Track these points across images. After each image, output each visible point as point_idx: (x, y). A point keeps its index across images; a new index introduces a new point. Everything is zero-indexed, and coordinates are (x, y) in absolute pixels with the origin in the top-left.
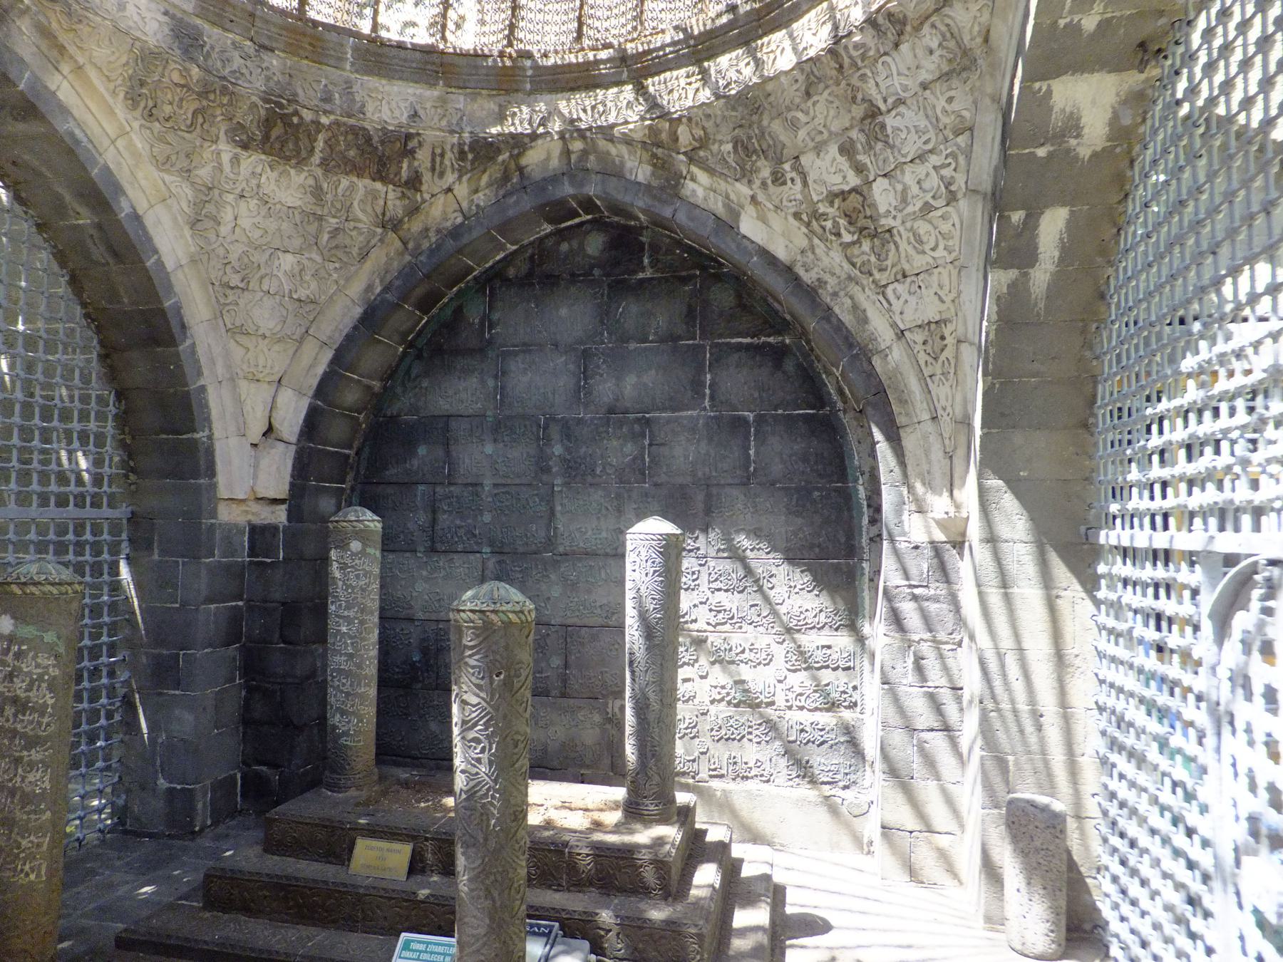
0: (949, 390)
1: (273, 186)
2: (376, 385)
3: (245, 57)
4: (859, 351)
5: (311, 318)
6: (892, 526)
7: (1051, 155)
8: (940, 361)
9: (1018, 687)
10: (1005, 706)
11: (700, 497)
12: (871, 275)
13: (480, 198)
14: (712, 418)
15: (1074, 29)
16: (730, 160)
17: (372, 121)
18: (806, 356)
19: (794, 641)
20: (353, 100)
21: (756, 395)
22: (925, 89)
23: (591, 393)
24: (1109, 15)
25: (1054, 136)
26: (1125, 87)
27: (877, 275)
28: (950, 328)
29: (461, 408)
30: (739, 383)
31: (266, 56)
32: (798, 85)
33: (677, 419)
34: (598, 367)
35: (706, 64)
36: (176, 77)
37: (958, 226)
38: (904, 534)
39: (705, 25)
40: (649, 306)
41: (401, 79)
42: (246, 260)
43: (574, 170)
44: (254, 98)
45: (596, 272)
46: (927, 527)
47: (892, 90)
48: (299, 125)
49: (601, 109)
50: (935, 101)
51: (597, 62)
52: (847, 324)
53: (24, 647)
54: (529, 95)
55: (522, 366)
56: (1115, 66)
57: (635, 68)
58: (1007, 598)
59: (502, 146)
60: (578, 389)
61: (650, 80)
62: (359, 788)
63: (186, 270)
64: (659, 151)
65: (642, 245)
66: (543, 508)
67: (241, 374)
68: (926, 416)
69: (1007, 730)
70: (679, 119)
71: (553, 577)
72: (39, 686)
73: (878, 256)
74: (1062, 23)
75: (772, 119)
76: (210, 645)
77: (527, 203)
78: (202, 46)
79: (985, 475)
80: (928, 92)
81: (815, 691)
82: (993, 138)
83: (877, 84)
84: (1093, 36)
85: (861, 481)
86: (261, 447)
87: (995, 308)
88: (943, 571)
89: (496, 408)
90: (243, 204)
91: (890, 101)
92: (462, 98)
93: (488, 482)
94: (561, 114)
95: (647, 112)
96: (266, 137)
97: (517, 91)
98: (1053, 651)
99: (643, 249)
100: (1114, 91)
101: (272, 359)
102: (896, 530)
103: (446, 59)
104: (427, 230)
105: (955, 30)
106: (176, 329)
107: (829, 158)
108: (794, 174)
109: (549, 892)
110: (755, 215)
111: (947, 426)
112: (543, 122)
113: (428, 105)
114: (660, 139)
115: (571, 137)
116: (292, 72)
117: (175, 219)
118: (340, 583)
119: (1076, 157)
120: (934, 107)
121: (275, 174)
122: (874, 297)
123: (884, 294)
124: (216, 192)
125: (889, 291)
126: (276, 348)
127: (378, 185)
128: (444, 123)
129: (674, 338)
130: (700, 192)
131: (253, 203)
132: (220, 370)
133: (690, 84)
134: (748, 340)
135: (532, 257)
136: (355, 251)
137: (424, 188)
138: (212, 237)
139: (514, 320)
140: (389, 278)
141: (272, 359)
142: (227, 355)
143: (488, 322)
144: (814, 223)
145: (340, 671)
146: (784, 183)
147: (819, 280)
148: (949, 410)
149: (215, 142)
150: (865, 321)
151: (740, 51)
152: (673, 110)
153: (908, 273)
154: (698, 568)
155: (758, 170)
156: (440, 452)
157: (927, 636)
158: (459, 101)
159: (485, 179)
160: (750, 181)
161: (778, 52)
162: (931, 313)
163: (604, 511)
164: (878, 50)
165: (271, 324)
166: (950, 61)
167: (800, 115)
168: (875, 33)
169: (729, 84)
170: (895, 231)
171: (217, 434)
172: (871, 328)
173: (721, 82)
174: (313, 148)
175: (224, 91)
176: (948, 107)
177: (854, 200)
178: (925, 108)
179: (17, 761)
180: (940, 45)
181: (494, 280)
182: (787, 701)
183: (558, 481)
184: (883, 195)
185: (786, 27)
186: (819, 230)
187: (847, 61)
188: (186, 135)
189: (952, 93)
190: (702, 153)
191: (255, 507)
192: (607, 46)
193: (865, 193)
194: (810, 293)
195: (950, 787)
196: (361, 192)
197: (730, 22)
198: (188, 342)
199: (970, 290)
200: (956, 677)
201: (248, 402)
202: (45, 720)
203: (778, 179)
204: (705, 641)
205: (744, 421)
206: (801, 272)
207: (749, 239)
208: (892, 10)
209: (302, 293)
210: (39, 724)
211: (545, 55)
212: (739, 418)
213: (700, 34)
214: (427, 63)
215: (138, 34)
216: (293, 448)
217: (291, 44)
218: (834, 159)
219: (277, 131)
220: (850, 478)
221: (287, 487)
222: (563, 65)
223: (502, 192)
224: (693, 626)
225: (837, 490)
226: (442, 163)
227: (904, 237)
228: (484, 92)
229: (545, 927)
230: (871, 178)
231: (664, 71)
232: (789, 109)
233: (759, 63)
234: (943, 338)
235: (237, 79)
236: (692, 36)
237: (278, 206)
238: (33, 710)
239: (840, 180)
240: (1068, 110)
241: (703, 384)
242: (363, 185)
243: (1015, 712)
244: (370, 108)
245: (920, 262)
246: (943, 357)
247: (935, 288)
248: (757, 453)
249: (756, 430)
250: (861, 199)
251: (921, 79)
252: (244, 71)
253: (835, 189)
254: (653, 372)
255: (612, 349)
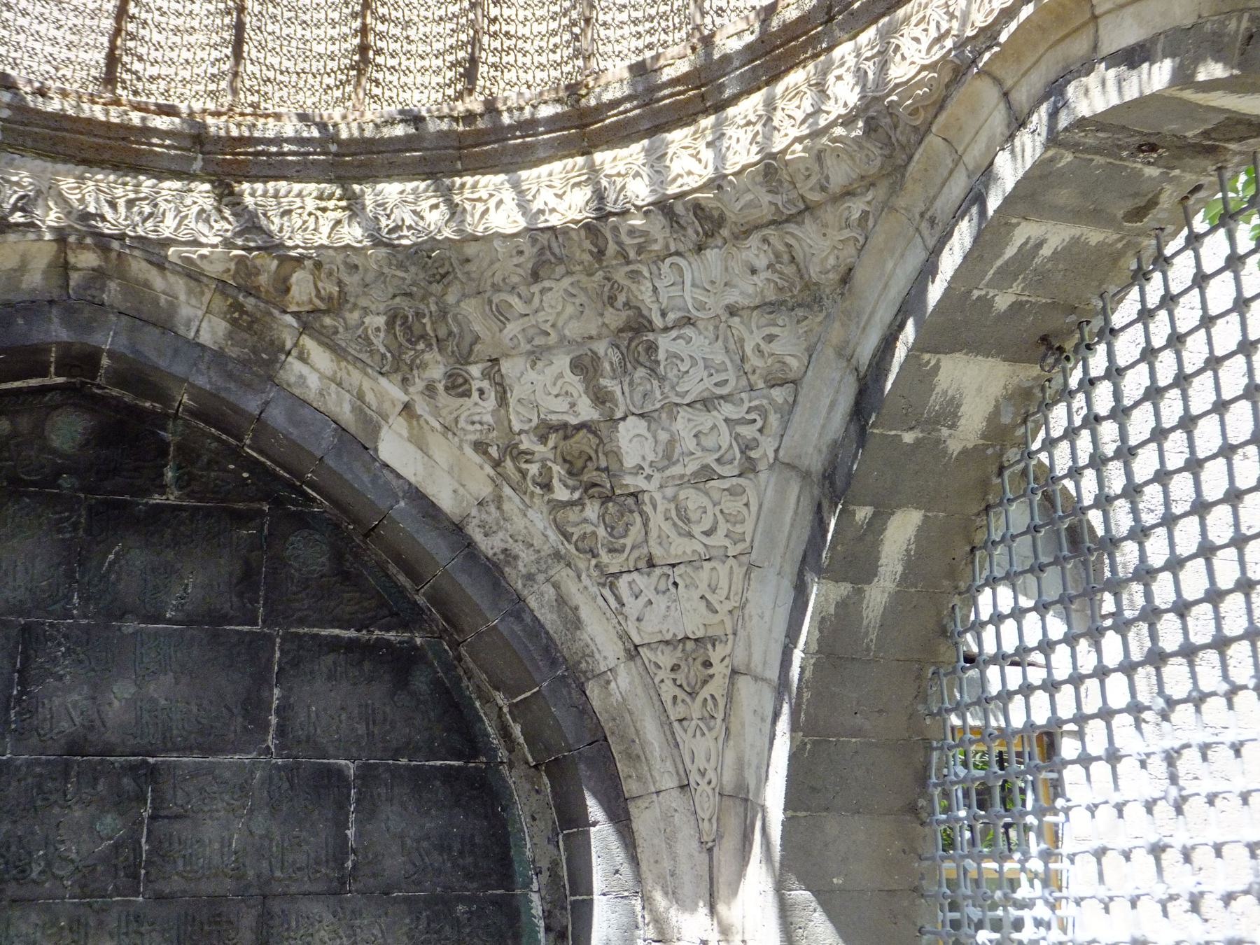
0: (712, 744)
4: (559, 668)
7: (918, 442)
8: (699, 699)
11: (248, 920)
15: (986, 302)
16: (379, 342)
18: (449, 668)
21: (361, 729)
22: (732, 314)
23: (33, 713)
24: (1025, 298)
25: (927, 421)
26: (1016, 380)
27: (605, 557)
30: (331, 708)
32: (522, 259)
33: (210, 770)
37: (754, 508)
40: (170, 555)
45: (66, 481)
47: (679, 302)
50: (746, 335)
52: (548, 626)
56: (1014, 355)
57: (223, 161)
64: (249, 303)
68: (669, 782)
70: (300, 260)
73: (611, 529)
74: (976, 293)
75: (464, 296)
79: (788, 884)
80: (737, 319)
82: (832, 405)
83: (655, 289)
84: (1002, 317)
85: (535, 886)
91: (672, 316)
94: (62, 200)
100: (1002, 384)
105: (799, 257)
107: (551, 372)
108: (485, 384)
110: (405, 433)
111: (706, 801)
114: (257, 284)
119: (945, 452)
120: (742, 340)
122: (594, 589)
123: (612, 587)
129: (216, 619)
130: (313, 381)
133: (324, 210)
134: (352, 633)
144: (509, 463)
146: (467, 394)
147: (505, 551)
148: (711, 774)
150: (577, 624)
153: (656, 561)
155: (423, 366)
161: (492, 203)
162: (692, 622)
164: (667, 247)
167: (514, 300)
170: (646, 497)
172: (585, 636)
176: (763, 346)
177: (583, 441)
178: (726, 340)
180: (770, 266)
184: (633, 443)
186: (516, 476)
187: (612, 248)
190: (328, 321)
192: (170, 111)
193: (604, 433)
194: (492, 572)
197: (408, 138)
199: (767, 600)
203: (457, 385)
205: (339, 773)
206: (478, 536)
207: (393, 471)
208: (703, 203)
211: (42, 92)
213: (351, 140)
218: (561, 375)
222: (77, 120)
225: (495, 901)
227: (660, 508)
230: (619, 415)
231: (277, 178)
232: (496, 288)
234: (707, 664)
236: (335, 139)
239: (565, 407)
240: (950, 393)
245: (681, 548)
246: (705, 693)
247: (703, 588)
248: (359, 835)
249: (359, 792)
251: (730, 300)
255: (87, 630)
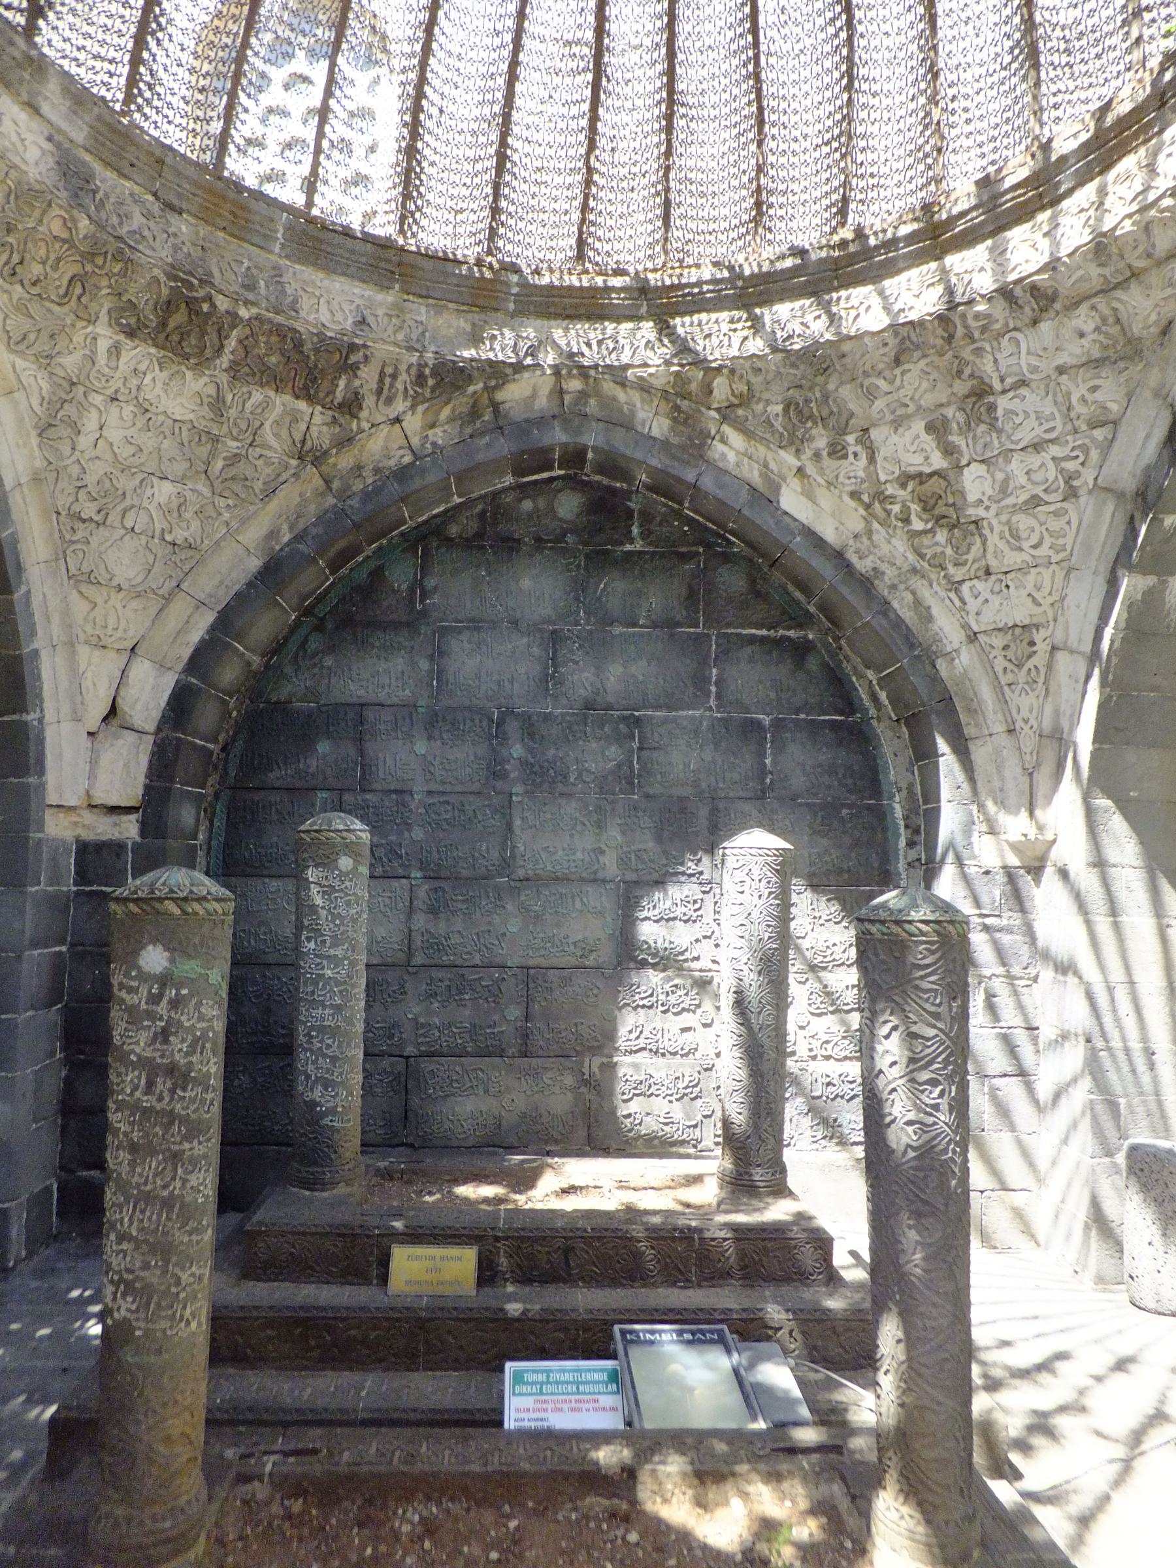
0: (1034, 700)
1: (159, 390)
2: (256, 660)
3: (148, 215)
5: (187, 568)
6: (960, 849)
8: (1025, 669)
9: (1130, 1023)
10: (1117, 1044)
11: (704, 812)
12: (943, 569)
13: (437, 435)
14: (720, 719)
16: (778, 424)
17: (307, 322)
19: (820, 980)
20: (283, 292)
21: (773, 695)
22: (1061, 373)
27: (951, 570)
28: (1043, 633)
29: (382, 696)
30: (752, 682)
31: (174, 218)
32: (887, 349)
33: (674, 720)
34: (572, 652)
35: (758, 311)
36: (57, 228)
37: (1074, 525)
38: (974, 857)
39: (760, 266)
41: (344, 274)
42: (107, 484)
43: (567, 412)
44: (156, 271)
45: (570, 538)
46: (1001, 850)
48: (208, 315)
49: (611, 346)
51: (607, 289)
52: (908, 621)
53: (185, 992)
54: (512, 317)
55: (466, 645)
57: (660, 304)
58: (1117, 926)
59: (475, 373)
60: (545, 678)
61: (678, 320)
62: (349, 1183)
63: (26, 491)
64: (685, 404)
65: (630, 514)
66: (497, 822)
67: (82, 637)
68: (999, 728)
69: (1118, 1070)
70: (719, 369)
71: (509, 907)
72: (203, 1047)
73: (956, 549)
75: (842, 383)
76: (33, 1008)
77: (503, 447)
78: (94, 192)
80: (1065, 377)
81: (844, 1038)
83: (996, 361)
85: (897, 799)
86: (100, 736)
87: (1125, 615)
88: (1017, 899)
89: (431, 697)
90: (114, 410)
91: (1009, 381)
92: (423, 309)
93: (419, 788)
94: (556, 345)
95: (674, 356)
96: (163, 324)
97: (496, 310)
98: (1164, 984)
99: (632, 517)
101: (127, 619)
102: (965, 853)
103: (410, 259)
104: (360, 468)
105: (1123, 316)
106: (11, 571)
107: (909, 435)
108: (859, 448)
109: (676, 1291)
111: (1028, 741)
112: (532, 351)
113: (380, 312)
114: (690, 390)
115: (569, 373)
116: (207, 245)
117: (20, 420)
118: (323, 913)
120: (1069, 394)
121: (165, 374)
122: (943, 594)
123: (957, 591)
124: (80, 390)
125: (965, 588)
126: (134, 604)
127: (302, 405)
128: (400, 336)
130: (732, 457)
131: (128, 410)
132: (56, 630)
133: (735, 330)
134: (764, 632)
135: (483, 514)
136: (258, 486)
137: (364, 414)
138: (67, 450)
139: (455, 589)
140: (301, 525)
141: (127, 619)
142: (66, 612)
143: (418, 588)
145: (322, 1029)
146: (845, 457)
147: (874, 569)
148: (1033, 722)
149: (92, 321)
150: (929, 618)
151: (807, 302)
152: (711, 358)
154: (701, 896)
155: (811, 439)
156: (351, 750)
157: (1001, 970)
158: (420, 311)
159: (446, 412)
160: (798, 451)
161: (862, 309)
162: (1021, 613)
163: (579, 828)
164: (1007, 324)
165: (131, 573)
166: (1106, 348)
167: (881, 383)
168: (1006, 305)
169: (790, 337)
170: (985, 523)
171: (49, 717)
172: (936, 628)
173: (779, 334)
174: (222, 346)
175: (118, 256)
176: (1090, 397)
177: (935, 485)
178: (1055, 395)
179: (175, 1158)
181: (428, 540)
182: (811, 1050)
183: (518, 789)
184: (975, 482)
185: (874, 283)
187: (960, 331)
188: (56, 308)
189: (1097, 382)
190: (740, 412)
191: (88, 817)
194: (865, 584)
195: (1024, 1137)
196: (279, 409)
198: (23, 589)
199: (1084, 596)
200: (1031, 1016)
201: (89, 674)
202: (209, 1096)
203: (837, 451)
204: (710, 982)
205: (759, 724)
206: (854, 559)
208: (1039, 284)
209: (179, 535)
210: (203, 1101)
212: (752, 721)
213: (753, 275)
214: (380, 259)
215: (16, 160)
216: (151, 739)
217: (207, 209)
218: (918, 436)
219: (178, 318)
220: (885, 795)
221: (140, 791)
223: (468, 430)
224: (695, 965)
225: (869, 808)
226: (391, 386)
227: (996, 530)
228: (451, 305)
229: (711, 1332)
230: (964, 462)
231: (699, 311)
232: (866, 374)
233: (833, 318)
234: (1032, 643)
235: (137, 242)
236: (741, 276)
237: (161, 418)
238: (197, 1082)
241: (706, 680)
242: (282, 401)
243: (1127, 1050)
244: (305, 304)
245: (1013, 559)
247: (1030, 588)
248: (774, 762)
250: (944, 484)
252: (146, 233)
253: (912, 470)
254: (644, 663)
255: (591, 632)
